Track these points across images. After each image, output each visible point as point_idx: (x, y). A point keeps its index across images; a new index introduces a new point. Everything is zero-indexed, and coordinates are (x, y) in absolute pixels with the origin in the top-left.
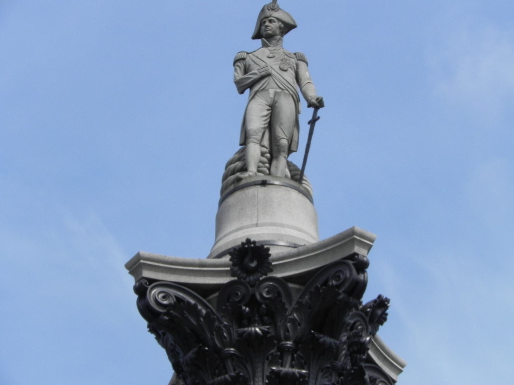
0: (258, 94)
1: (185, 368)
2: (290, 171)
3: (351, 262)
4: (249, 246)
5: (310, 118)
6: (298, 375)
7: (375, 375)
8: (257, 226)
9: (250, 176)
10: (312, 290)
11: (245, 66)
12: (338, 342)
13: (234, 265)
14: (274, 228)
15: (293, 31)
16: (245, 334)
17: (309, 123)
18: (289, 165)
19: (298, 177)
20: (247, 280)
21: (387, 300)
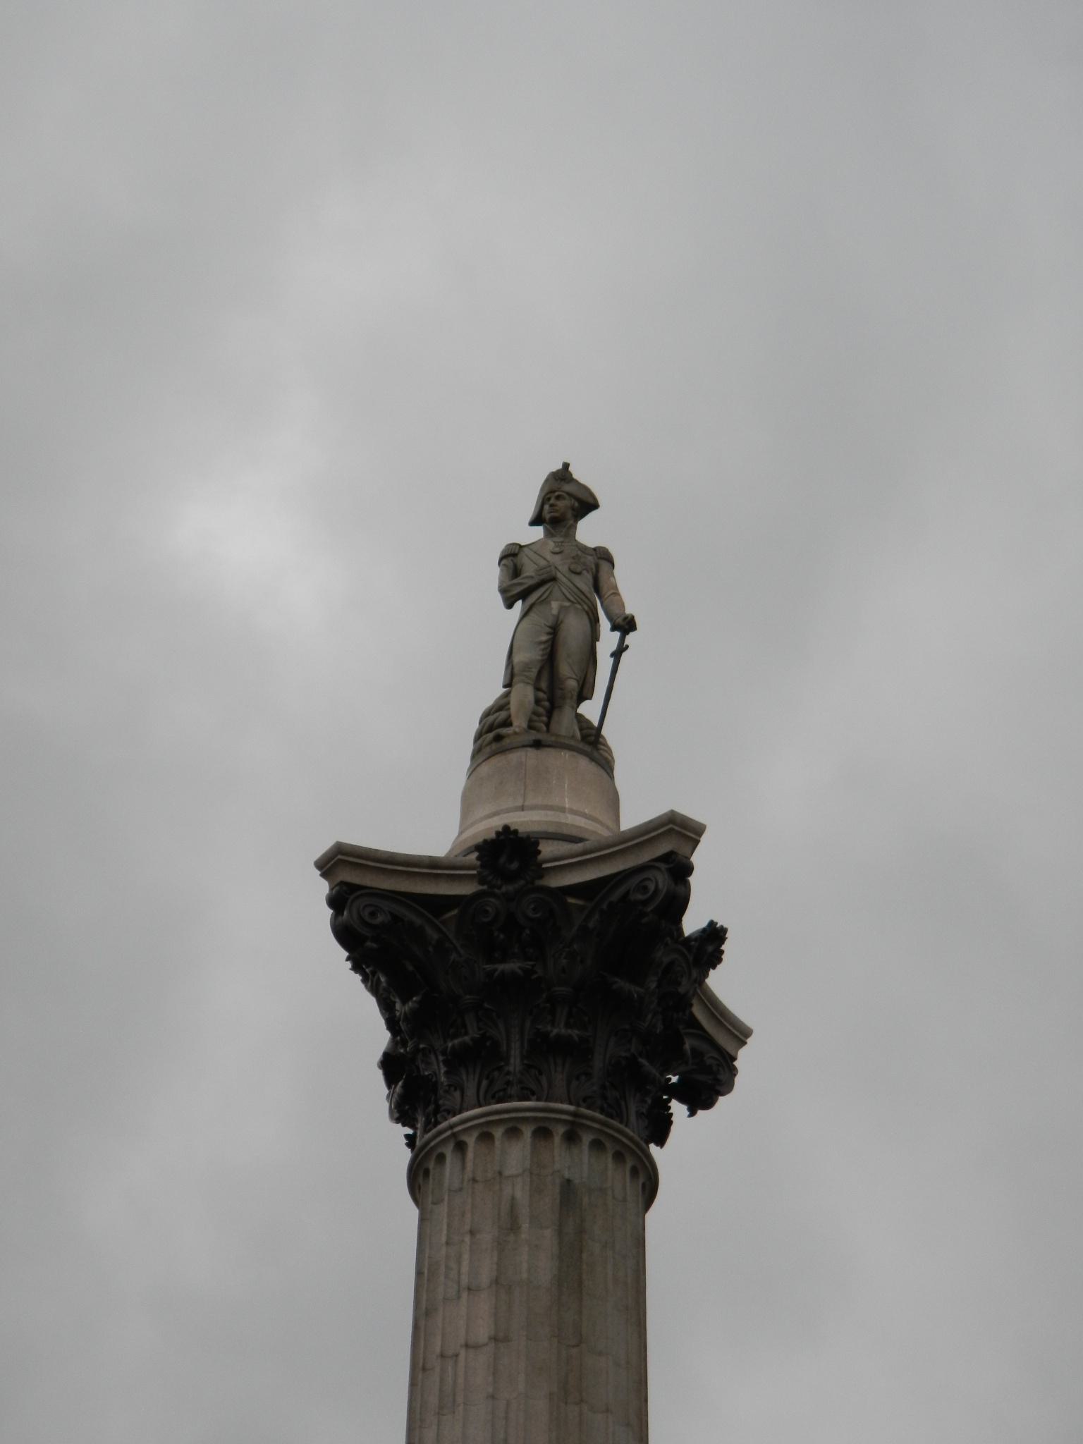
0: (534, 609)
1: (403, 1026)
2: (581, 730)
3: (663, 866)
5: (614, 647)
6: (520, 972)
7: (704, 1047)
9: (515, 733)
10: (605, 906)
11: (515, 566)
12: (641, 990)
13: (482, 866)
14: (549, 813)
15: (592, 516)
17: (612, 655)
18: (580, 718)
19: (593, 738)
20: (504, 889)
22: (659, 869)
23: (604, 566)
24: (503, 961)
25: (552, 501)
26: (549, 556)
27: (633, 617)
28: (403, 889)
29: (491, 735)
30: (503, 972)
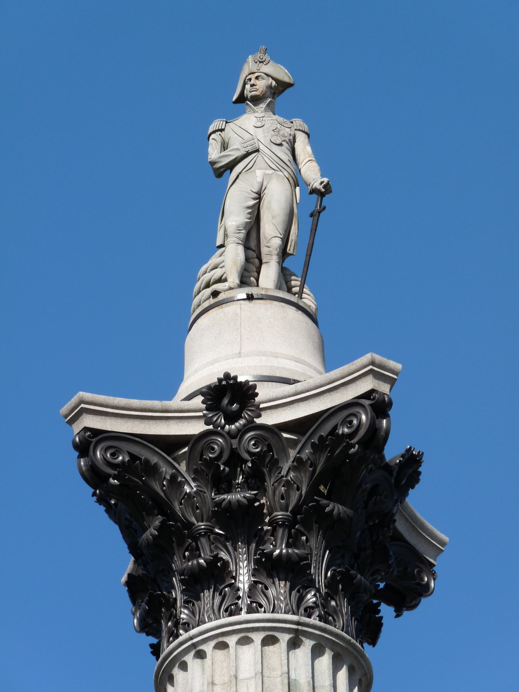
3: (366, 402)
4: (227, 382)
6: (245, 501)
8: (240, 357)
10: (315, 440)
13: (207, 409)
16: (224, 504)
21: (420, 455)
22: (362, 406)
23: (201, 494)
24: (229, 491)
25: (252, 82)
26: (252, 130)
27: (227, 376)
28: (139, 432)
29: (208, 291)
30: (230, 502)
